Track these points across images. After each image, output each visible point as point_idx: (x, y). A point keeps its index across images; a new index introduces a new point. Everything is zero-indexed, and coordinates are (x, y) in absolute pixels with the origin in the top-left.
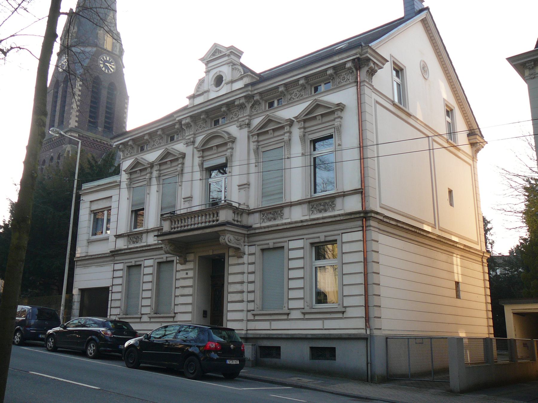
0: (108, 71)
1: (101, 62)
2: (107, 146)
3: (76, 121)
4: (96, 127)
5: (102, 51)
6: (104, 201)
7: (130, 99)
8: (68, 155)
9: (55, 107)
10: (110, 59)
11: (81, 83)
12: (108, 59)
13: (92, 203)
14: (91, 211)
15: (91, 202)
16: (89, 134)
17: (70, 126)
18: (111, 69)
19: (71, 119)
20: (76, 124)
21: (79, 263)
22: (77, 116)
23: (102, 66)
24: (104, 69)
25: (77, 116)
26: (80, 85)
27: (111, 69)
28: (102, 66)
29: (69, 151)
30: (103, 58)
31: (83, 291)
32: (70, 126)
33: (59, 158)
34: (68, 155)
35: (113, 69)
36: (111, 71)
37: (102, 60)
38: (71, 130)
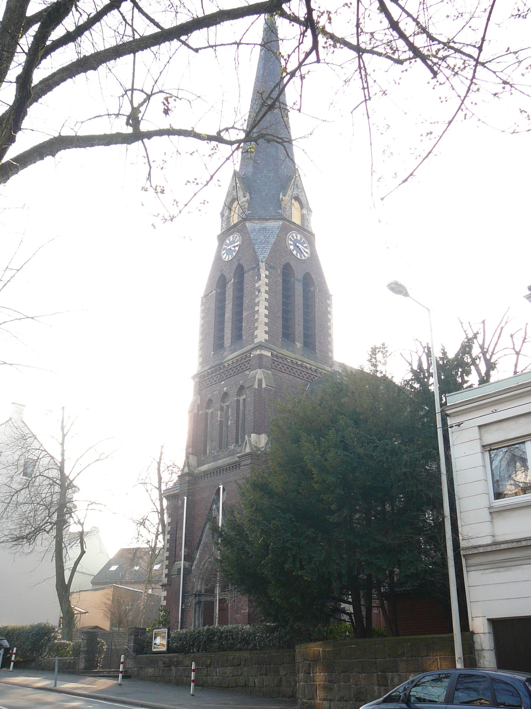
0: (301, 257)
1: (290, 242)
2: (310, 371)
3: (266, 332)
4: (294, 341)
5: (288, 226)
6: (522, 420)
7: (334, 299)
8: (260, 384)
9: (223, 315)
10: (301, 239)
11: (267, 273)
12: (299, 238)
13: (484, 430)
14: (483, 446)
15: (480, 427)
16: (285, 352)
17: (256, 341)
18: (305, 253)
19: (257, 328)
20: (266, 337)
21: (472, 561)
22: (266, 324)
23: (292, 247)
24: (295, 252)
25: (266, 324)
26: (266, 276)
27: (305, 253)
28: (292, 247)
29: (260, 381)
30: (293, 236)
31: (497, 625)
32: (256, 341)
33: (239, 393)
34: (260, 384)
35: (307, 253)
36: (305, 256)
37: (291, 240)
38: (260, 346)
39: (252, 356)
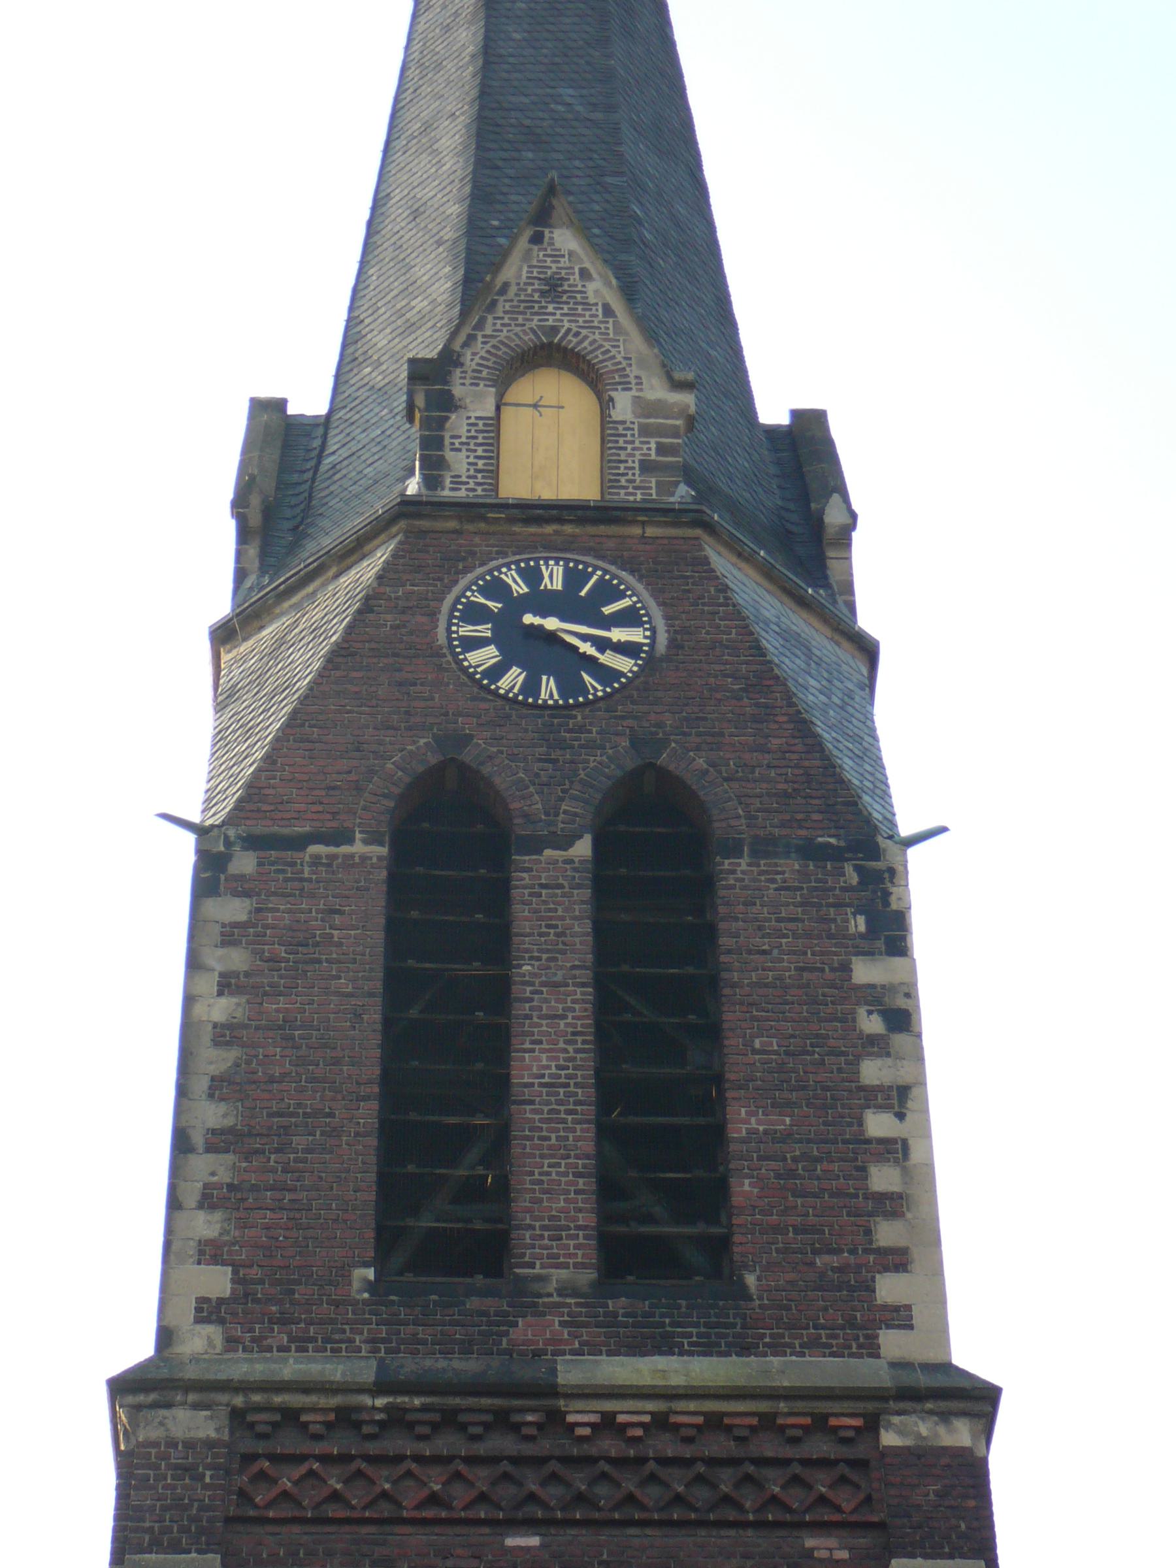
39: (889, 1439)
